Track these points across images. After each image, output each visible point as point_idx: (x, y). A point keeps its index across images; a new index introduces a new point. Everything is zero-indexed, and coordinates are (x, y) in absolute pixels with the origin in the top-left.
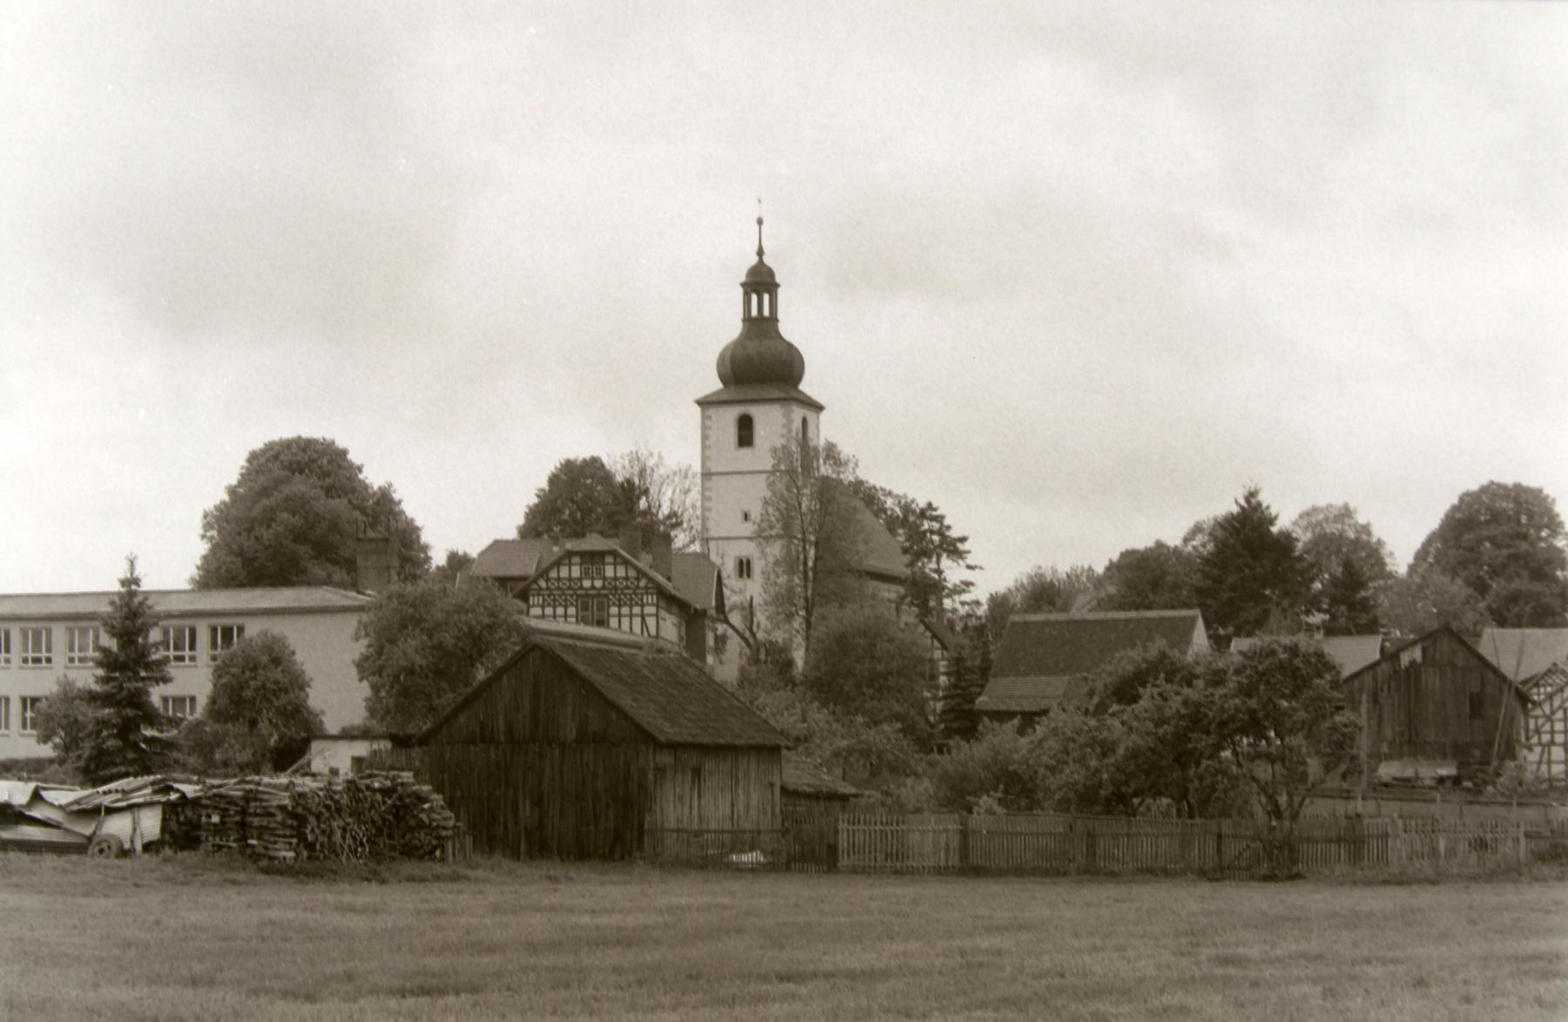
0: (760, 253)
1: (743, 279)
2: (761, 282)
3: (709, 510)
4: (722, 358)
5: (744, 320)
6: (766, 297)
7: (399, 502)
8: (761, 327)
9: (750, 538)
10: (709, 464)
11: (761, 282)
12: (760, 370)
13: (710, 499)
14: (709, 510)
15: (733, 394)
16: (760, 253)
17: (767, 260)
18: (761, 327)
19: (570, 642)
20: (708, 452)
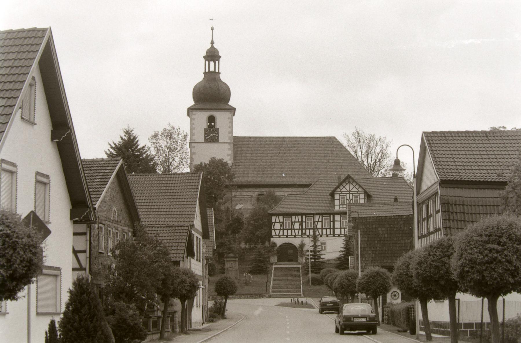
0: (212, 43)
1: (205, 54)
2: (212, 56)
3: (194, 153)
4: (196, 87)
5: (205, 73)
6: (217, 62)
7: (201, 163)
8: (212, 77)
9: (482, 320)
10: (194, 137)
11: (212, 56)
12: (211, 96)
13: (194, 129)
14: (194, 153)
15: (199, 106)
16: (212, 43)
17: (215, 46)
18: (212, 77)
19: (353, 332)
20: (193, 131)
